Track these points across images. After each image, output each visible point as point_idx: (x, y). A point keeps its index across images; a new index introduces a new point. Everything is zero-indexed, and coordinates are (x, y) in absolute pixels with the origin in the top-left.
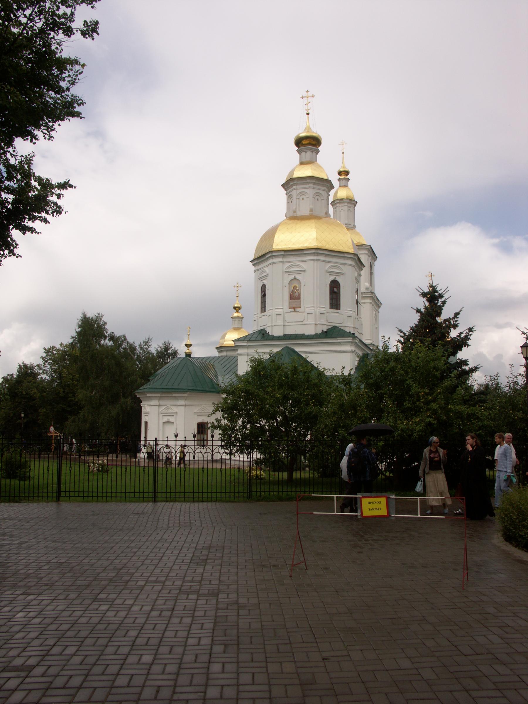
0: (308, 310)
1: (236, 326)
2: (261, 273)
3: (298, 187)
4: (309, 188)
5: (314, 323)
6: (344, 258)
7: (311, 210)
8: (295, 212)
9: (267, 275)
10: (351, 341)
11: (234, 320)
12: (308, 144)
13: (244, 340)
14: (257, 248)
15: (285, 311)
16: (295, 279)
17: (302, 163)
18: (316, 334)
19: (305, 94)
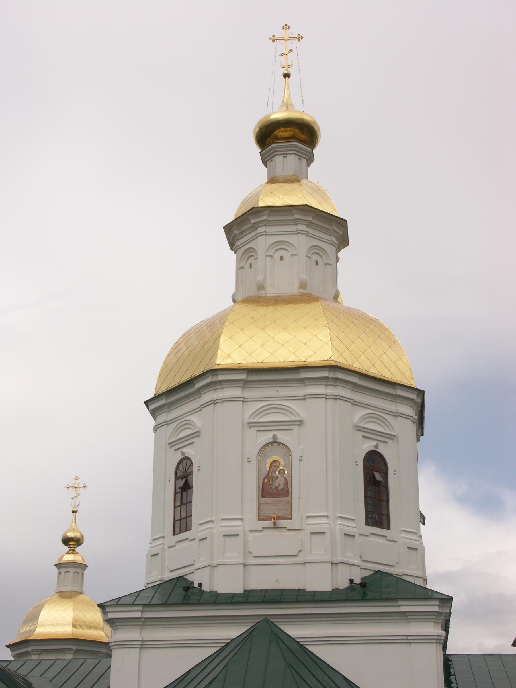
0: (313, 525)
1: (69, 588)
2: (177, 430)
3: (269, 229)
4: (298, 233)
5: (328, 558)
6: (395, 398)
7: (303, 285)
8: (261, 287)
9: (197, 434)
10: (436, 609)
11: (63, 570)
12: (287, 138)
13: (133, 605)
14: (162, 370)
15: (248, 528)
16: (275, 442)
17: (272, 180)
18: (336, 591)
19: (279, 33)
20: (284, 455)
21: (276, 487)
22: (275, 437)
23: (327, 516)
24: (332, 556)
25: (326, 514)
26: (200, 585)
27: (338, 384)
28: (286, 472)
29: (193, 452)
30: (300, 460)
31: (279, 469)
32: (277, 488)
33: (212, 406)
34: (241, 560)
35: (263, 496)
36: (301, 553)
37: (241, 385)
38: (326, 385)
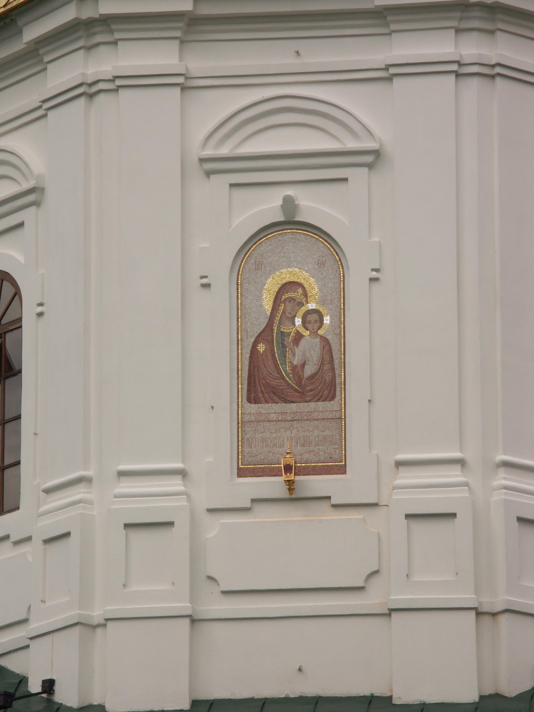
5: (467, 597)
15: (203, 500)
16: (290, 223)
20: (321, 264)
21: (294, 368)
22: (289, 204)
23: (461, 462)
24: (477, 591)
25: (457, 455)
26: (49, 686)
27: (500, 26)
28: (327, 320)
29: (21, 259)
30: (373, 280)
31: (303, 309)
32: (297, 371)
33: (82, 101)
34: (183, 605)
35: (253, 398)
36: (376, 580)
37: (178, 34)
38: (458, 31)
